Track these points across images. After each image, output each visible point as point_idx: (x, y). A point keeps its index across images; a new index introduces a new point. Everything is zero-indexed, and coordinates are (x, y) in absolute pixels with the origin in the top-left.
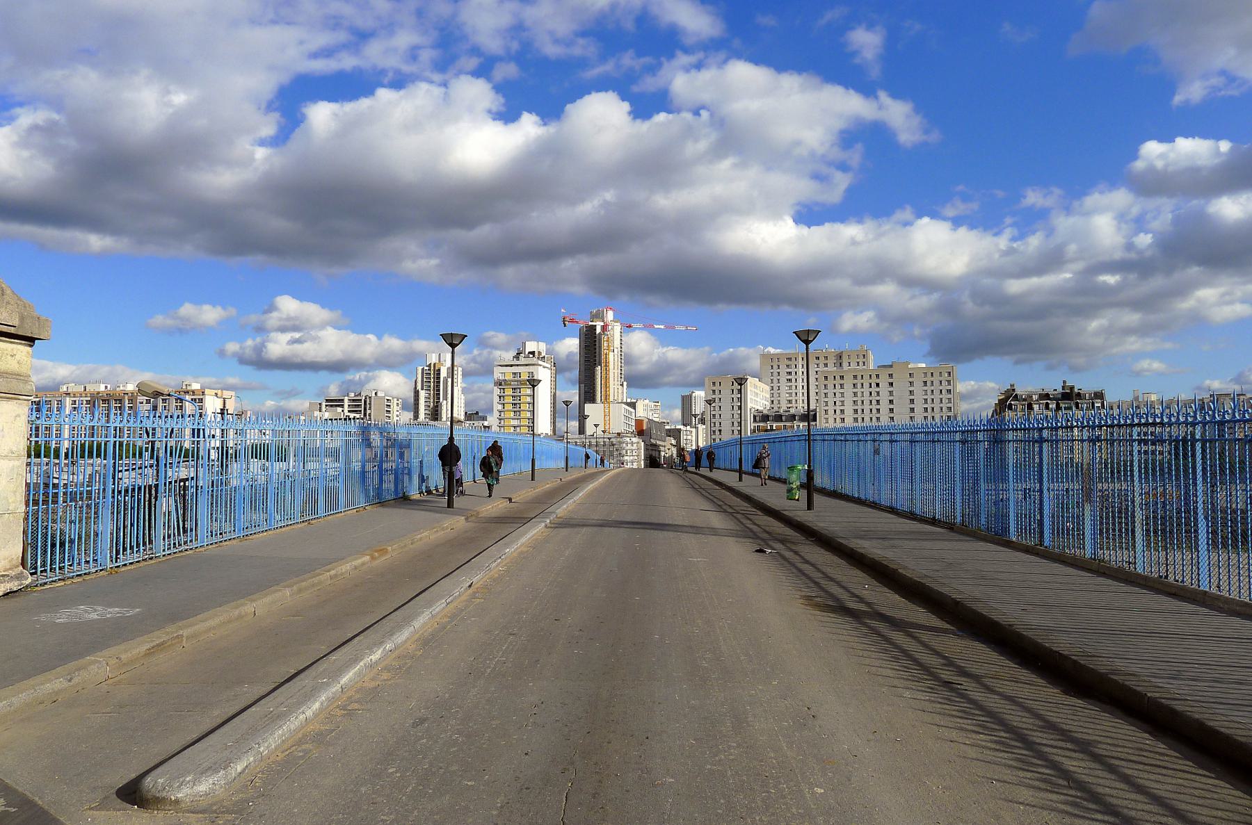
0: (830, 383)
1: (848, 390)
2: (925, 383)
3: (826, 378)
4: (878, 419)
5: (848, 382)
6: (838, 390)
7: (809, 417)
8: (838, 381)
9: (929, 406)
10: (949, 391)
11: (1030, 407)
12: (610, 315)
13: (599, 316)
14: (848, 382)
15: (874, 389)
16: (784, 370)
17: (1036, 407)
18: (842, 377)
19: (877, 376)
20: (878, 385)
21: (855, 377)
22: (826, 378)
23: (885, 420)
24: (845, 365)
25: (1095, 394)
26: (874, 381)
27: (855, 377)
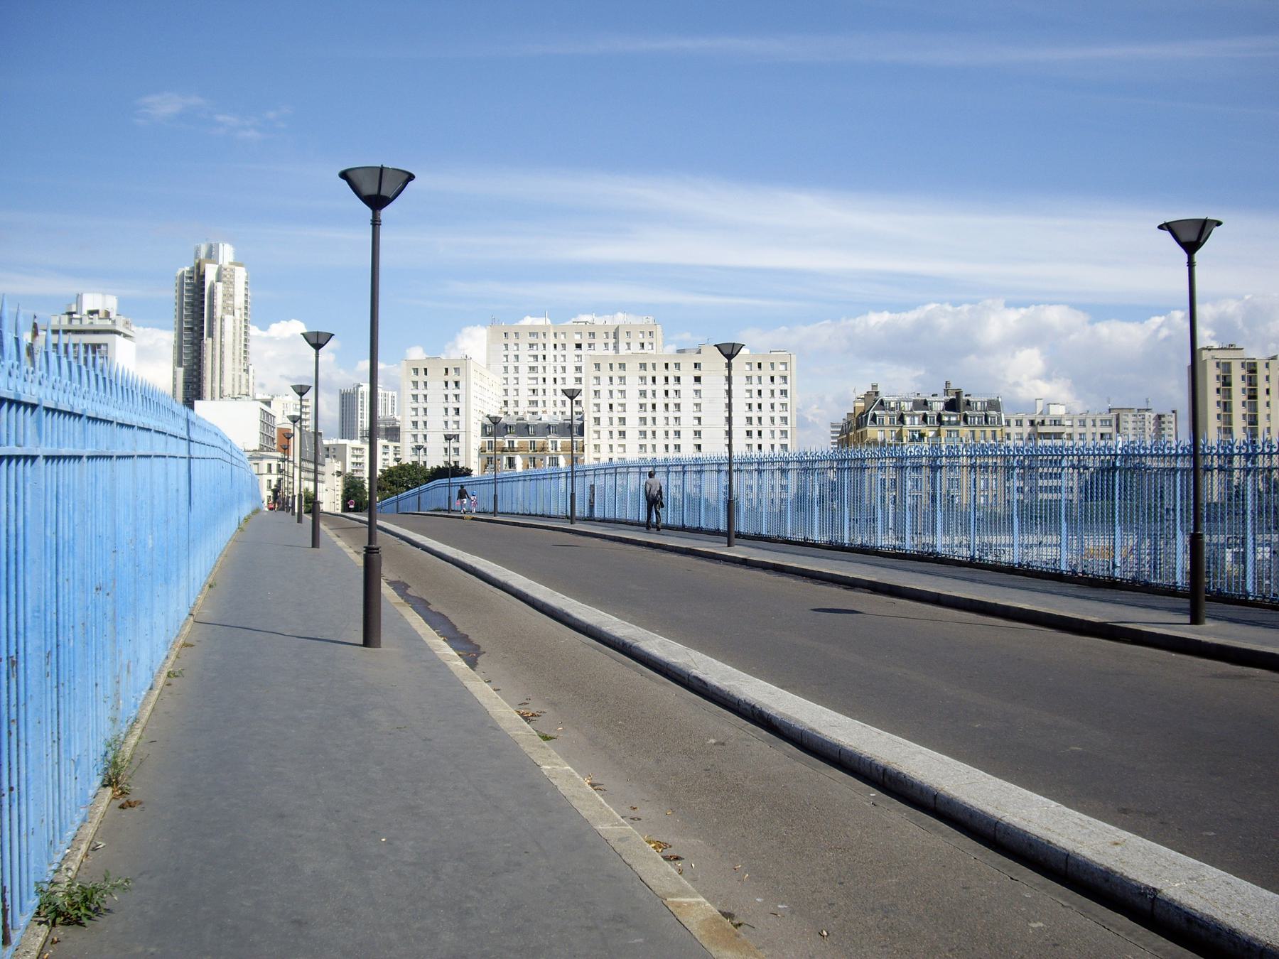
0: (605, 374)
1: (633, 386)
2: (749, 378)
3: (598, 366)
4: (678, 447)
5: (632, 373)
6: (616, 386)
7: (573, 429)
8: (617, 373)
9: (755, 414)
10: (784, 392)
11: (901, 419)
12: (226, 254)
13: (211, 255)
14: (632, 373)
15: (672, 386)
16: (524, 352)
17: (907, 419)
18: (622, 366)
19: (677, 365)
20: (678, 379)
21: (643, 366)
22: (598, 366)
23: (688, 443)
24: (622, 346)
25: (990, 402)
26: (672, 373)
27: (643, 366)
